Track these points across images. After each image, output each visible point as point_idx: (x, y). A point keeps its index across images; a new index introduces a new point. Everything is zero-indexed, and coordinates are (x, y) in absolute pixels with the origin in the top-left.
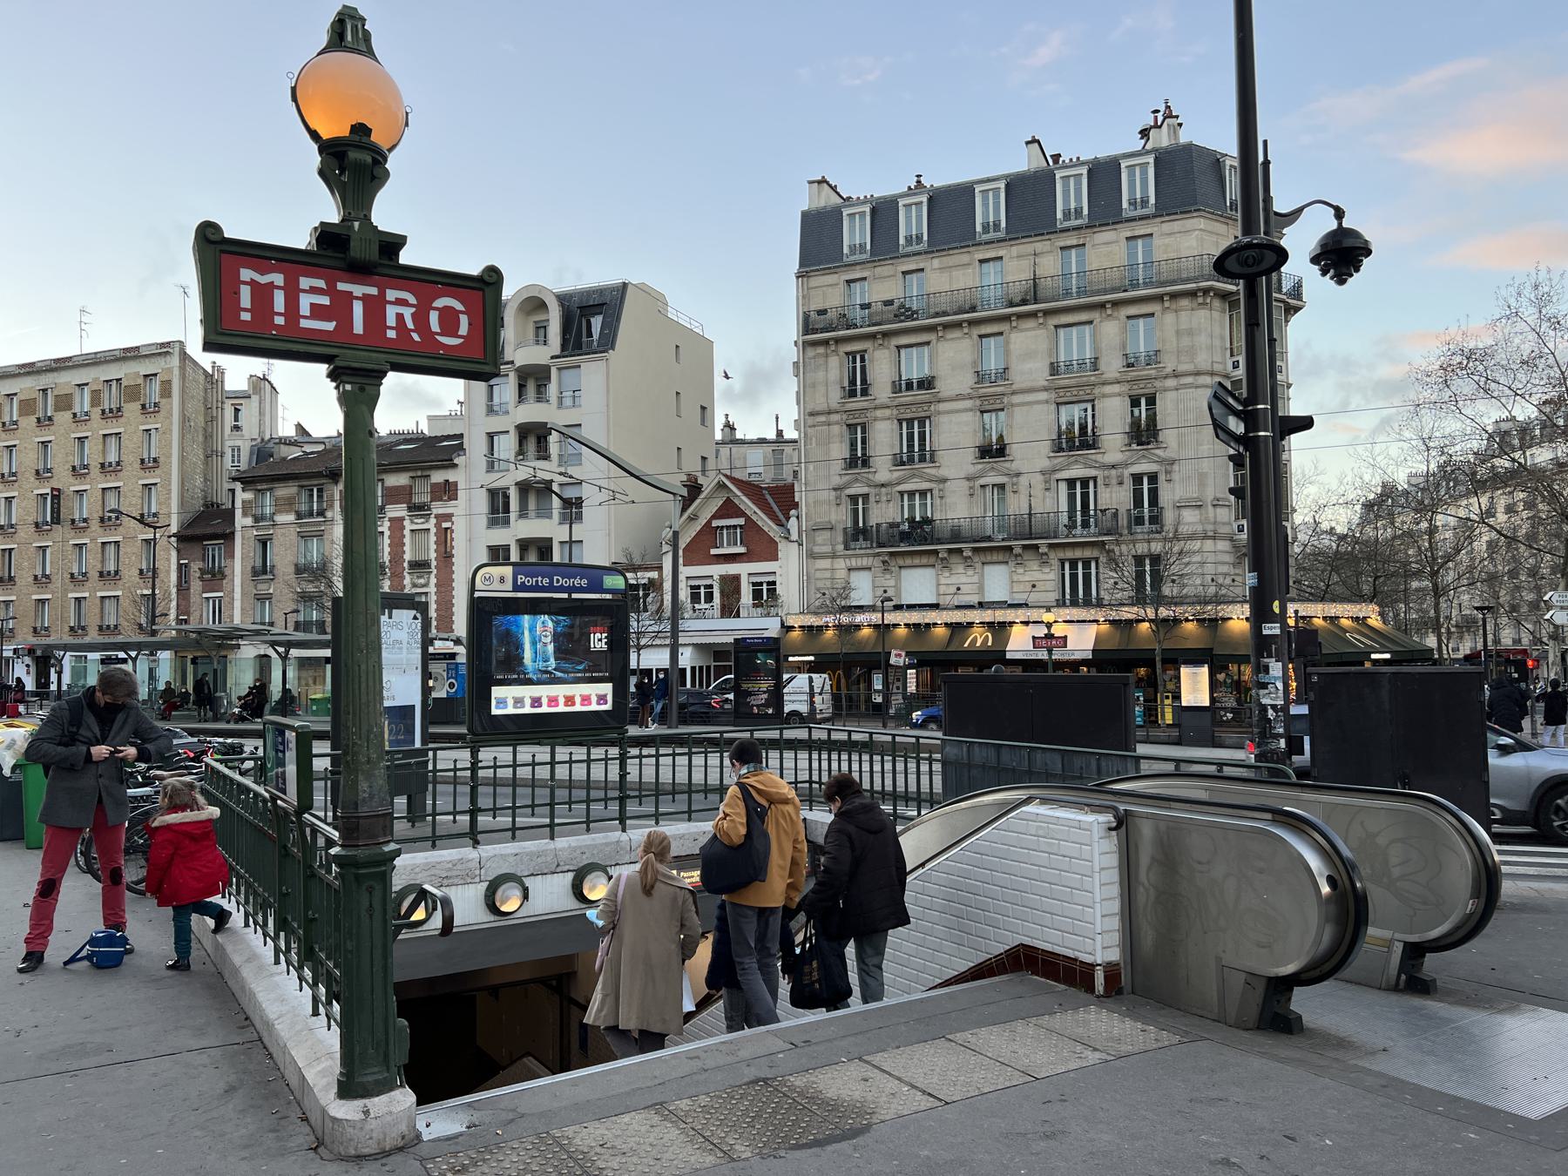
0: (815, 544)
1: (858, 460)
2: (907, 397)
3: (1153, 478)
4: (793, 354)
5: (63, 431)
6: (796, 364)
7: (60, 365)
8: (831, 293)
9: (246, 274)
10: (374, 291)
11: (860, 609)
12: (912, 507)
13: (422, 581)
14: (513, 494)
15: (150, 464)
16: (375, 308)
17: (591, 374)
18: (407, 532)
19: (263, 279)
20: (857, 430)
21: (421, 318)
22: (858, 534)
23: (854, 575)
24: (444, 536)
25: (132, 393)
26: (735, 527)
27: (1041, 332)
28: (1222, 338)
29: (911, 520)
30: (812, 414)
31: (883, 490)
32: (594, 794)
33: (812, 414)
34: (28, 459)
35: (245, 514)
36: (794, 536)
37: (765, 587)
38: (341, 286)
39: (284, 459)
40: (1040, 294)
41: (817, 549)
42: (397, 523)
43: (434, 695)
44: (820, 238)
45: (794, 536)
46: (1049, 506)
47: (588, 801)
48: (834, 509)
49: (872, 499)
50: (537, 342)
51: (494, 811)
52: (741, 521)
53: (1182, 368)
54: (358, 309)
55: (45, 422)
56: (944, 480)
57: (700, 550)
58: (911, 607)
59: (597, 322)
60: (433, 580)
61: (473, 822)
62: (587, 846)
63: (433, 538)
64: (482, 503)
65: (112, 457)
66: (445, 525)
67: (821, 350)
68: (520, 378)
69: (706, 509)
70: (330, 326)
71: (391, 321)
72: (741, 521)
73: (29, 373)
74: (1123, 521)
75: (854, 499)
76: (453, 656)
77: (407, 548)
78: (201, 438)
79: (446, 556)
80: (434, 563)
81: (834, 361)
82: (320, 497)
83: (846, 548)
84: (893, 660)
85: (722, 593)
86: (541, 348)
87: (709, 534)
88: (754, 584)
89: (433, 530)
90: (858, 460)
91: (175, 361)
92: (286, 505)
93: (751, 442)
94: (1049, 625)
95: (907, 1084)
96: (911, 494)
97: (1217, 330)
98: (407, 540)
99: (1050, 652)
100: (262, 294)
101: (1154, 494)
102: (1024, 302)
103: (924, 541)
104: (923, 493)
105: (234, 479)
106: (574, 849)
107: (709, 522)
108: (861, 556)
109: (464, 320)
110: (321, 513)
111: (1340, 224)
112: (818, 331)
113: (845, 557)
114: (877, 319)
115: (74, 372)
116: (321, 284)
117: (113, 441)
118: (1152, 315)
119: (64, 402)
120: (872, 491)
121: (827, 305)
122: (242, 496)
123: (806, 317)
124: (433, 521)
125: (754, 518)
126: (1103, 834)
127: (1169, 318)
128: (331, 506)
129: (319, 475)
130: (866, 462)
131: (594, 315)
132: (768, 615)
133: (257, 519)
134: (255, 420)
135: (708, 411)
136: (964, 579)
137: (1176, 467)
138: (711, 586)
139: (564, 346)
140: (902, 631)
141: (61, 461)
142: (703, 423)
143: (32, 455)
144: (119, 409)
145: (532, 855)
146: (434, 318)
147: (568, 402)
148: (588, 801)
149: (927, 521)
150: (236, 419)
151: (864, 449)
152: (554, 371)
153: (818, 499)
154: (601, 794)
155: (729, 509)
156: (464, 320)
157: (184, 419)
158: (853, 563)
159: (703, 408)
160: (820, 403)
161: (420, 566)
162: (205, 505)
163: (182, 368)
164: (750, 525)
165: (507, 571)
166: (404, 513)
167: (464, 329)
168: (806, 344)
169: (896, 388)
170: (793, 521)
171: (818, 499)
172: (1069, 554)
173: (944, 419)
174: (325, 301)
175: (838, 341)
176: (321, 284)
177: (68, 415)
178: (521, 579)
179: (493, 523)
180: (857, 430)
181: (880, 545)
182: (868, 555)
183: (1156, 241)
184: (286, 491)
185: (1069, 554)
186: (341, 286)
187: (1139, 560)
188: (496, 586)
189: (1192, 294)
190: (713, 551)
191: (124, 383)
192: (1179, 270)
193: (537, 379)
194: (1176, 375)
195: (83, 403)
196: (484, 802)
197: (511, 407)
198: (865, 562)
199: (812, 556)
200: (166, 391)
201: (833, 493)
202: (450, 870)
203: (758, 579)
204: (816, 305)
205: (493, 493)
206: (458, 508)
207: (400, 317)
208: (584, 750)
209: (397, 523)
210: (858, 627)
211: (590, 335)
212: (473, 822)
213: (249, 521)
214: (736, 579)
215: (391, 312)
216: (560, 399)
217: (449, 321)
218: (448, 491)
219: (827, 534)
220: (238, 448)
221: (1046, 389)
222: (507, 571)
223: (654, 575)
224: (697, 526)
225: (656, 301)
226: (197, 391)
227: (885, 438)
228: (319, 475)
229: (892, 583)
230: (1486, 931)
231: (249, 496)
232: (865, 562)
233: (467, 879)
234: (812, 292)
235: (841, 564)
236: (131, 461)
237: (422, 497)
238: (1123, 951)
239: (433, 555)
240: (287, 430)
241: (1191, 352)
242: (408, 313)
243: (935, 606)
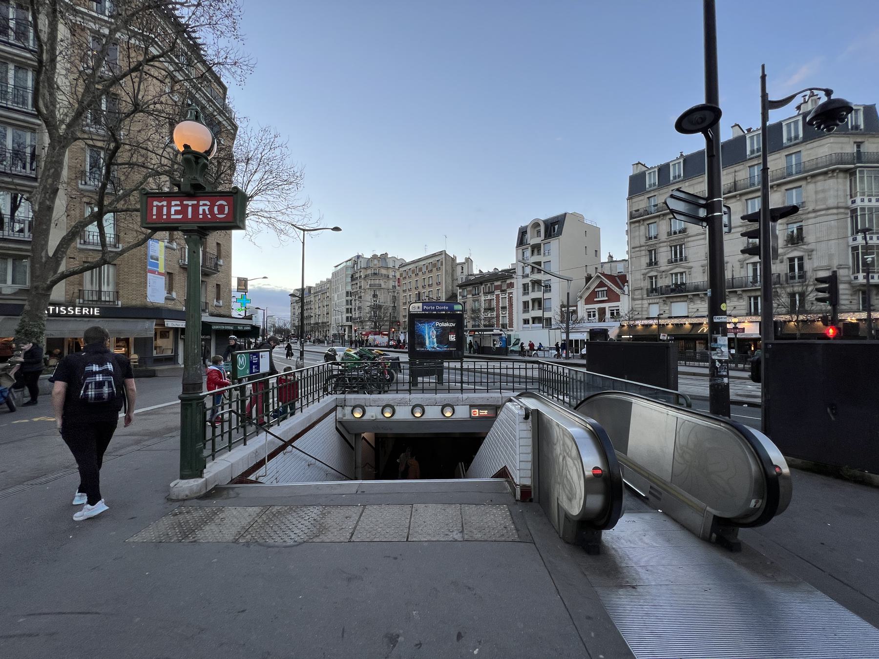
2: (674, 237)
3: (801, 259)
6: (627, 231)
8: (642, 203)
9: (155, 203)
10: (195, 202)
11: (653, 318)
12: (676, 279)
14: (530, 284)
16: (195, 208)
19: (160, 204)
20: (652, 252)
21: (211, 210)
22: (653, 291)
24: (510, 299)
25: (434, 265)
27: (739, 203)
28: (845, 191)
29: (676, 284)
34: (413, 285)
38: (185, 202)
40: (738, 187)
42: (498, 296)
44: (637, 185)
45: (627, 292)
46: (743, 274)
53: (818, 208)
54: (190, 209)
56: (691, 268)
57: (589, 301)
58: (675, 317)
59: (556, 227)
64: (521, 290)
67: (637, 224)
70: (180, 217)
71: (201, 212)
74: (783, 278)
75: (651, 278)
79: (511, 305)
81: (642, 228)
84: (661, 337)
87: (594, 294)
92: (470, 292)
94: (735, 324)
96: (676, 274)
97: (841, 187)
99: (736, 334)
100: (160, 209)
101: (801, 267)
102: (729, 192)
103: (682, 292)
104: (682, 273)
109: (227, 208)
111: (829, 98)
112: (636, 218)
116: (178, 203)
118: (800, 187)
119: (420, 270)
122: (460, 291)
123: (631, 213)
126: (522, 420)
127: (811, 187)
130: (656, 264)
136: (700, 306)
137: (814, 253)
141: (420, 285)
146: (216, 208)
149: (682, 284)
153: (636, 279)
154: (518, 380)
155: (601, 284)
156: (227, 208)
157: (446, 271)
158: (651, 301)
161: (504, 308)
164: (610, 290)
167: (226, 212)
169: (669, 234)
171: (636, 279)
172: (753, 294)
173: (690, 244)
174: (179, 208)
175: (644, 220)
176: (178, 203)
179: (524, 294)
180: (652, 252)
181: (662, 294)
183: (803, 153)
185: (753, 294)
186: (185, 202)
187: (792, 295)
188: (417, 310)
189: (825, 173)
192: (817, 164)
194: (814, 211)
195: (424, 269)
198: (656, 301)
199: (633, 299)
200: (442, 265)
207: (204, 210)
209: (498, 296)
210: (651, 325)
214: (604, 308)
215: (201, 209)
217: (221, 209)
218: (511, 285)
220: (461, 278)
221: (741, 226)
225: (579, 218)
227: (664, 255)
230: (757, 528)
232: (656, 301)
235: (645, 302)
237: (504, 287)
238: (534, 480)
240: (476, 272)
241: (825, 199)
242: (206, 208)
243: (687, 317)
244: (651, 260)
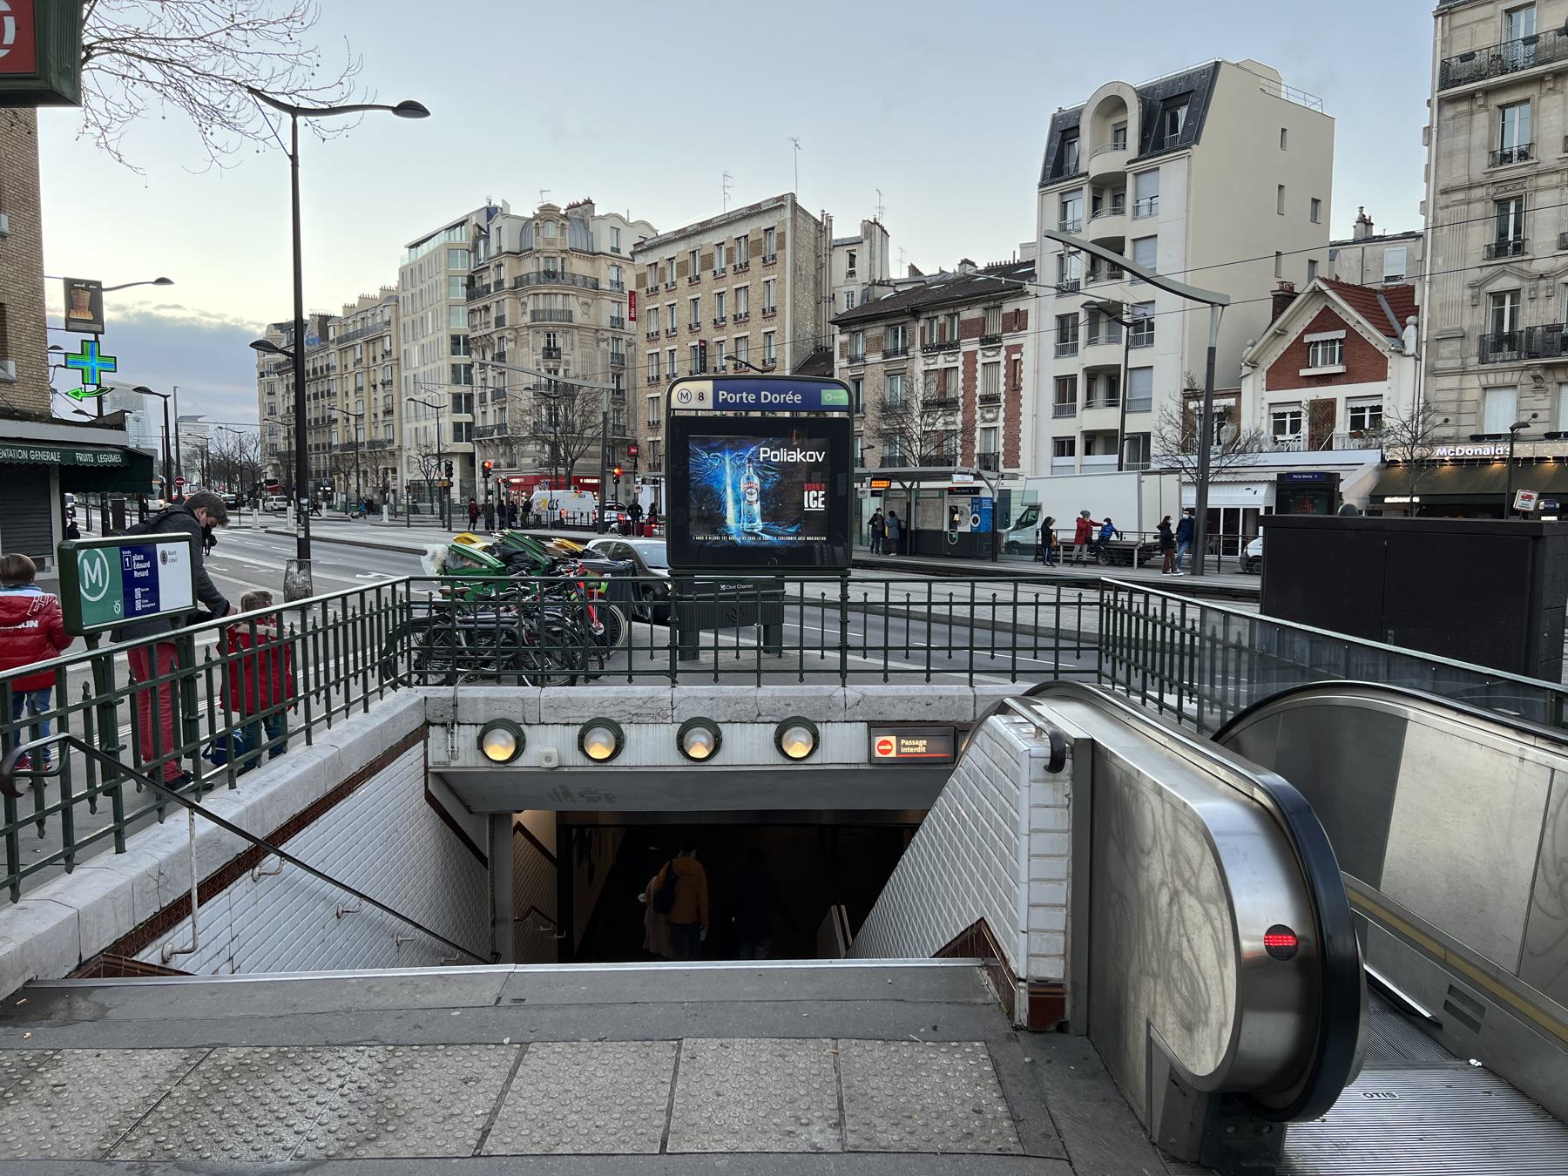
0: (1438, 358)
1: (1507, 247)
4: (1425, 117)
5: (707, 288)
7: (704, 228)
13: (989, 416)
15: (770, 313)
17: (1172, 175)
18: (979, 366)
22: (1503, 343)
23: (1492, 396)
24: (1014, 368)
25: (756, 247)
26: (1333, 341)
30: (1445, 192)
31: (1542, 282)
32: (1022, 640)
33: (1445, 192)
34: (683, 316)
35: (842, 356)
36: (1411, 349)
37: (1367, 414)
39: (878, 300)
41: (1440, 364)
43: (960, 529)
45: (1411, 349)
47: (1014, 649)
48: (1467, 311)
49: (1524, 295)
50: (1116, 147)
51: (865, 650)
52: (1341, 334)
55: (695, 281)
57: (1281, 375)
59: (1182, 113)
60: (1002, 415)
61: (843, 660)
62: (795, 698)
63: (1003, 371)
65: (742, 310)
66: (1014, 357)
67: (1463, 107)
68: (1095, 190)
69: (1299, 319)
72: (1341, 334)
73: (682, 238)
75: (1498, 297)
76: (977, 490)
77: (979, 383)
78: (812, 286)
79: (1015, 389)
80: (1003, 397)
81: (1481, 119)
82: (904, 337)
83: (1482, 361)
84: (1518, 504)
85: (1312, 423)
86: (1121, 153)
87: (1300, 352)
88: (1354, 410)
89: (1003, 363)
90: (1507, 247)
91: (788, 213)
93: (1394, 238)
95: (509, 1081)
98: (979, 375)
105: (833, 323)
106: (778, 700)
107: (1301, 337)
108: (1504, 370)
110: (905, 352)
113: (1478, 373)
114: (1548, 55)
115: (713, 233)
117: (742, 294)
119: (708, 262)
120: (1527, 285)
121: (1475, 47)
123: (1445, 66)
124: (1003, 352)
125: (1358, 329)
126: (1041, 774)
128: (913, 344)
129: (902, 313)
130: (1519, 248)
131: (1178, 106)
132: (1367, 447)
133: (852, 360)
134: (866, 265)
135: (1322, 205)
138: (1299, 414)
139: (1142, 149)
140: (1551, 465)
141: (706, 316)
142: (1314, 218)
143: (686, 312)
144: (747, 264)
145: (729, 701)
147: (1144, 211)
148: (1014, 649)
150: (852, 264)
151: (1517, 230)
152: (1130, 177)
153: (1448, 302)
154: (1051, 643)
155: (1327, 320)
157: (796, 268)
159: (1316, 201)
160: (1458, 176)
162: (816, 349)
163: (794, 219)
165: (707, 386)
166: (977, 347)
168: (1443, 102)
170: (1410, 330)
175: (1488, 92)
177: (710, 273)
178: (722, 395)
181: (1531, 355)
182: (1512, 370)
184: (875, 331)
188: (694, 404)
190: (1303, 372)
191: (750, 239)
193: (1114, 190)
195: (720, 262)
196: (854, 636)
197: (1083, 224)
198: (1509, 378)
199: (1433, 372)
200: (781, 245)
201: (1469, 292)
202: (640, 707)
203: (1359, 404)
204: (1460, 49)
205: (1062, 319)
206: (1027, 340)
208: (1054, 590)
209: (970, 358)
211: (1174, 129)
212: (843, 660)
213: (845, 363)
214: (1331, 404)
216: (1136, 209)
218: (1018, 321)
219: (1456, 344)
220: (846, 293)
222: (707, 386)
223: (1232, 401)
224: (1286, 343)
225: (1261, 80)
226: (808, 240)
228: (902, 313)
229: (1546, 404)
231: (845, 338)
232: (1509, 378)
233: (658, 718)
234: (1456, 33)
235: (1473, 382)
236: (756, 311)
237: (994, 328)
239: (1002, 389)
240: (898, 272)
244: (1502, 234)
